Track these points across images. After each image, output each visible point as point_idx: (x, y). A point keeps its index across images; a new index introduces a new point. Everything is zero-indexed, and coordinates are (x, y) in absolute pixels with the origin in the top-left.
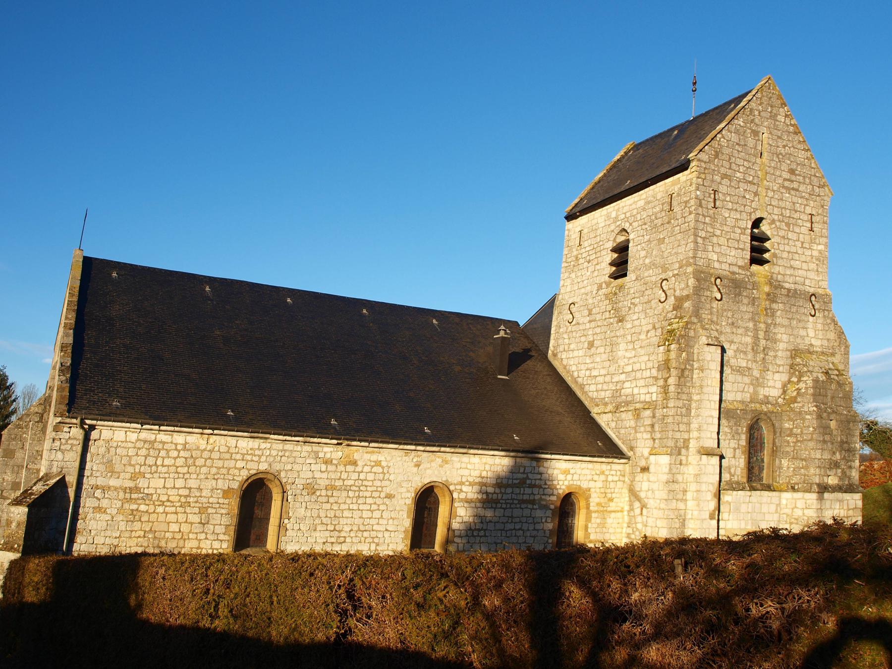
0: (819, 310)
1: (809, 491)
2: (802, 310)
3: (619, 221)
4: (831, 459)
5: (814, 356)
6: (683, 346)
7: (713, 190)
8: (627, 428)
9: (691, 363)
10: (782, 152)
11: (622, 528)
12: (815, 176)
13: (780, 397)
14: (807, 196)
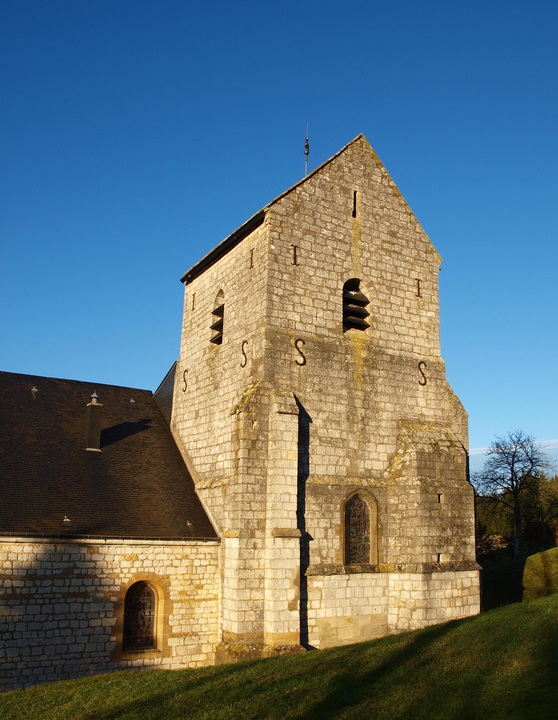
0: (430, 378)
1: (415, 572)
2: (410, 378)
3: (218, 281)
4: (440, 536)
5: (425, 427)
6: (254, 414)
7: (292, 246)
8: (218, 506)
9: (266, 433)
10: (380, 212)
11: (217, 618)
12: (420, 240)
13: (386, 470)
14: (412, 260)
